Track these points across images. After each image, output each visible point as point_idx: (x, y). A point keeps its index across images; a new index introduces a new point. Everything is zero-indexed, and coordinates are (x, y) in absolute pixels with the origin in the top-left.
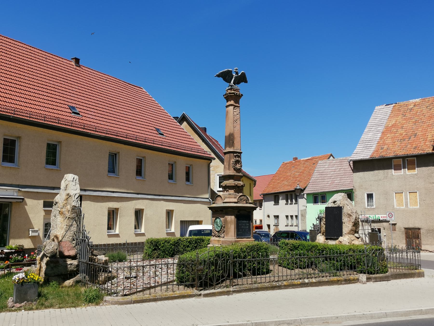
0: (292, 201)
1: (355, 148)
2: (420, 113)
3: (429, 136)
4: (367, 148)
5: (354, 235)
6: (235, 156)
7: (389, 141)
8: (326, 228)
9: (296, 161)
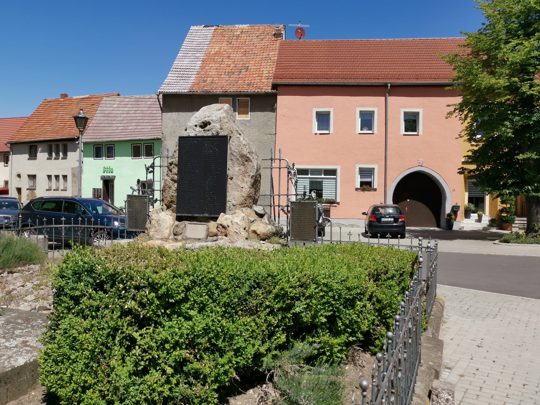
0: (57, 154)
1: (165, 77)
2: (250, 43)
3: (264, 72)
4: (183, 78)
5: (251, 207)
7: (213, 73)
8: (178, 190)
9: (66, 98)
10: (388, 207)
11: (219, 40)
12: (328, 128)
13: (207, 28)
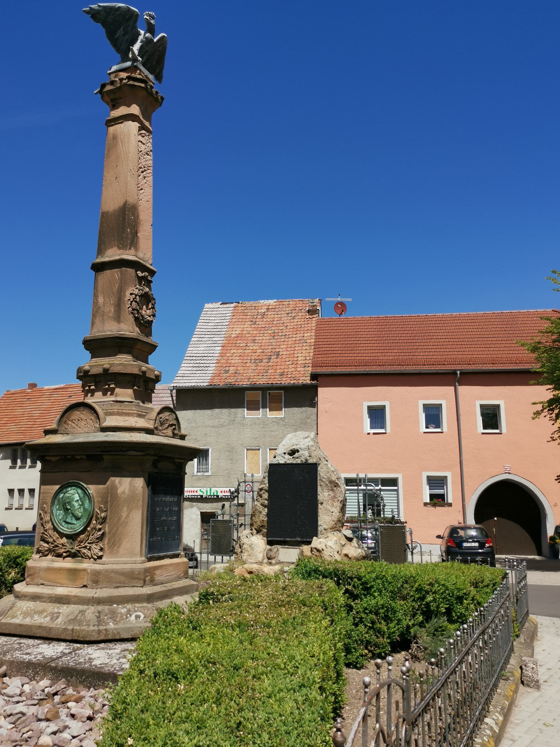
0: (24, 462)
1: (178, 367)
3: (300, 359)
4: (201, 369)
5: (340, 531)
6: (140, 279)
7: (236, 360)
8: (268, 515)
10: (470, 528)
11: (240, 320)
12: (383, 426)
13: (225, 306)
